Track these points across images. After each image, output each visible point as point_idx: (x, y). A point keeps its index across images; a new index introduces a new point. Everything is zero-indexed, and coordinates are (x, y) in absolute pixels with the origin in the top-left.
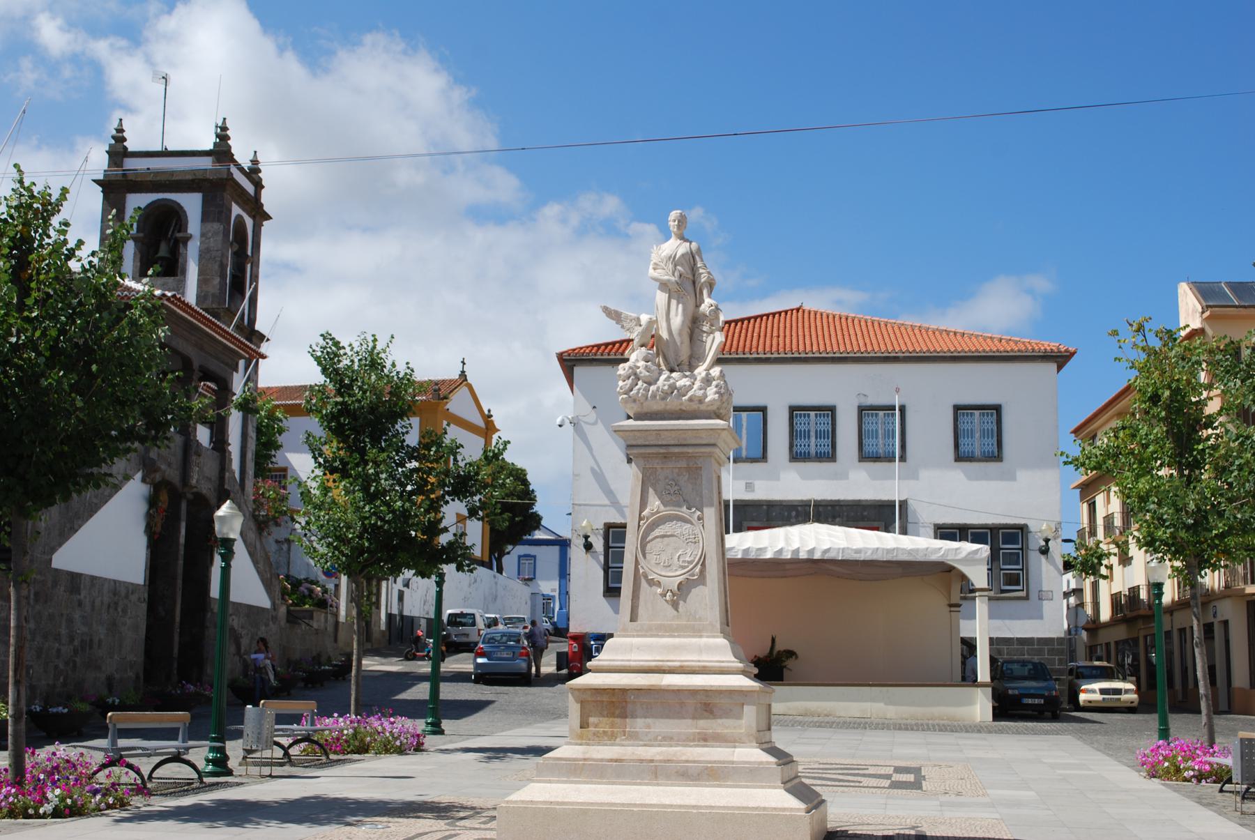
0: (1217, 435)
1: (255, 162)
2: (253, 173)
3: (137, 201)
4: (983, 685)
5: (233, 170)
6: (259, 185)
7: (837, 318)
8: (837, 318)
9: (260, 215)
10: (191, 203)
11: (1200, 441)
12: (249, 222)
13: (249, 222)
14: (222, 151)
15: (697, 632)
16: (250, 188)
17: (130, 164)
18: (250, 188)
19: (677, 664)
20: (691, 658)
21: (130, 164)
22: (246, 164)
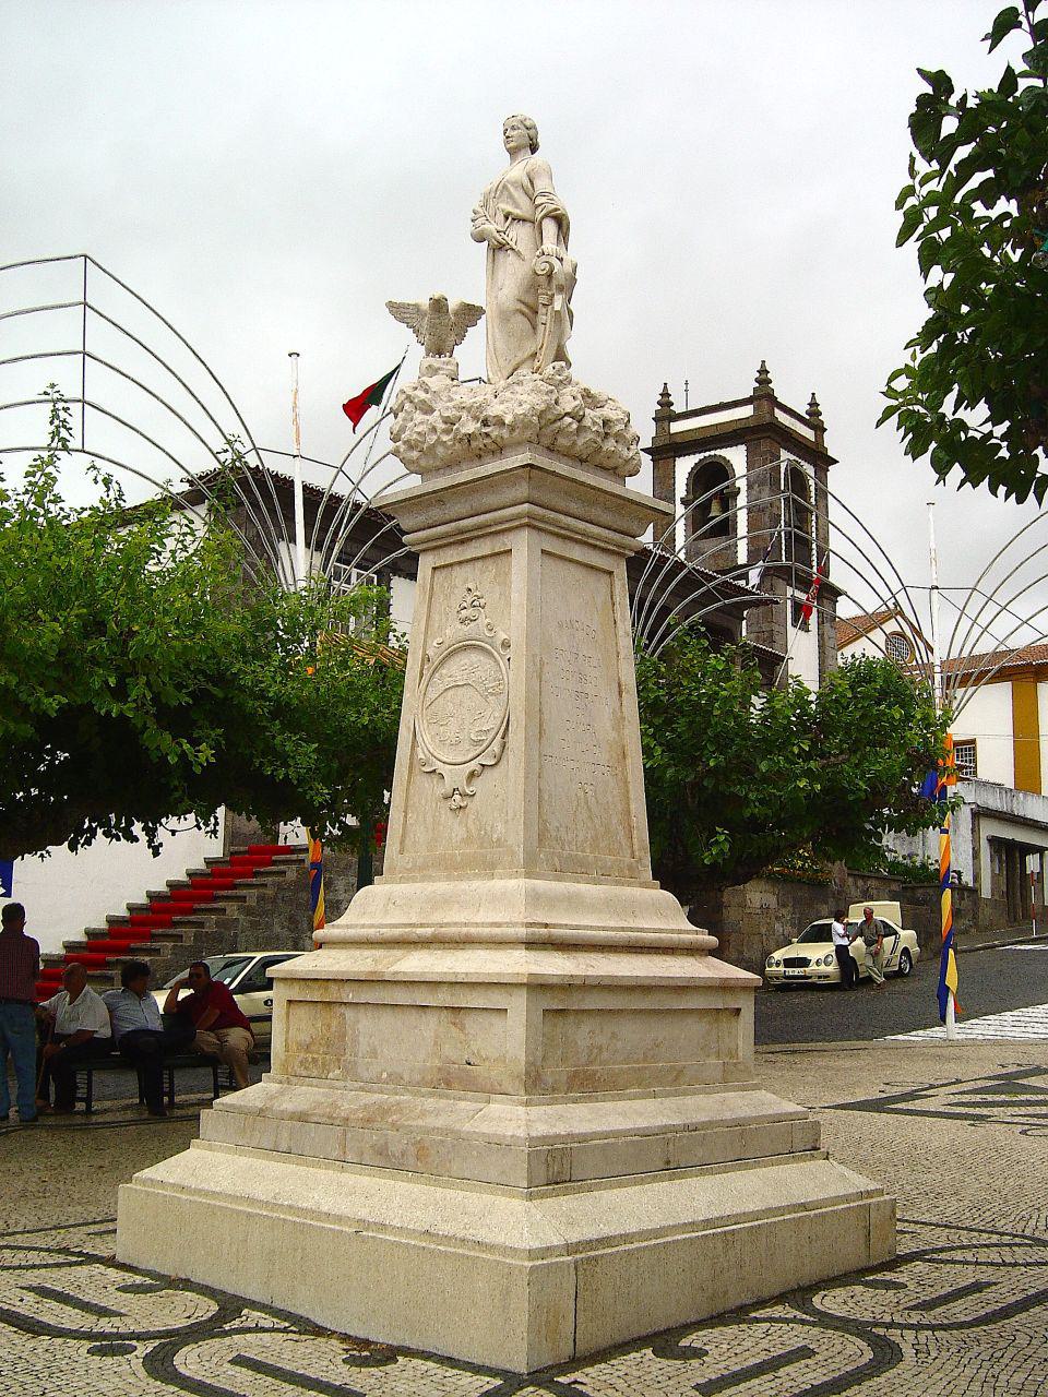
0: (666, 814)
1: (813, 404)
2: (814, 418)
3: (684, 466)
4: (971, 674)
5: (778, 413)
6: (819, 429)
7: (111, 1226)
8: (111, 1226)
9: (823, 461)
10: (736, 457)
11: (189, 704)
12: (809, 469)
13: (809, 469)
14: (764, 394)
15: (488, 868)
16: (809, 434)
17: (677, 427)
18: (809, 434)
19: (429, 931)
20: (455, 919)
21: (677, 427)
22: (802, 409)
